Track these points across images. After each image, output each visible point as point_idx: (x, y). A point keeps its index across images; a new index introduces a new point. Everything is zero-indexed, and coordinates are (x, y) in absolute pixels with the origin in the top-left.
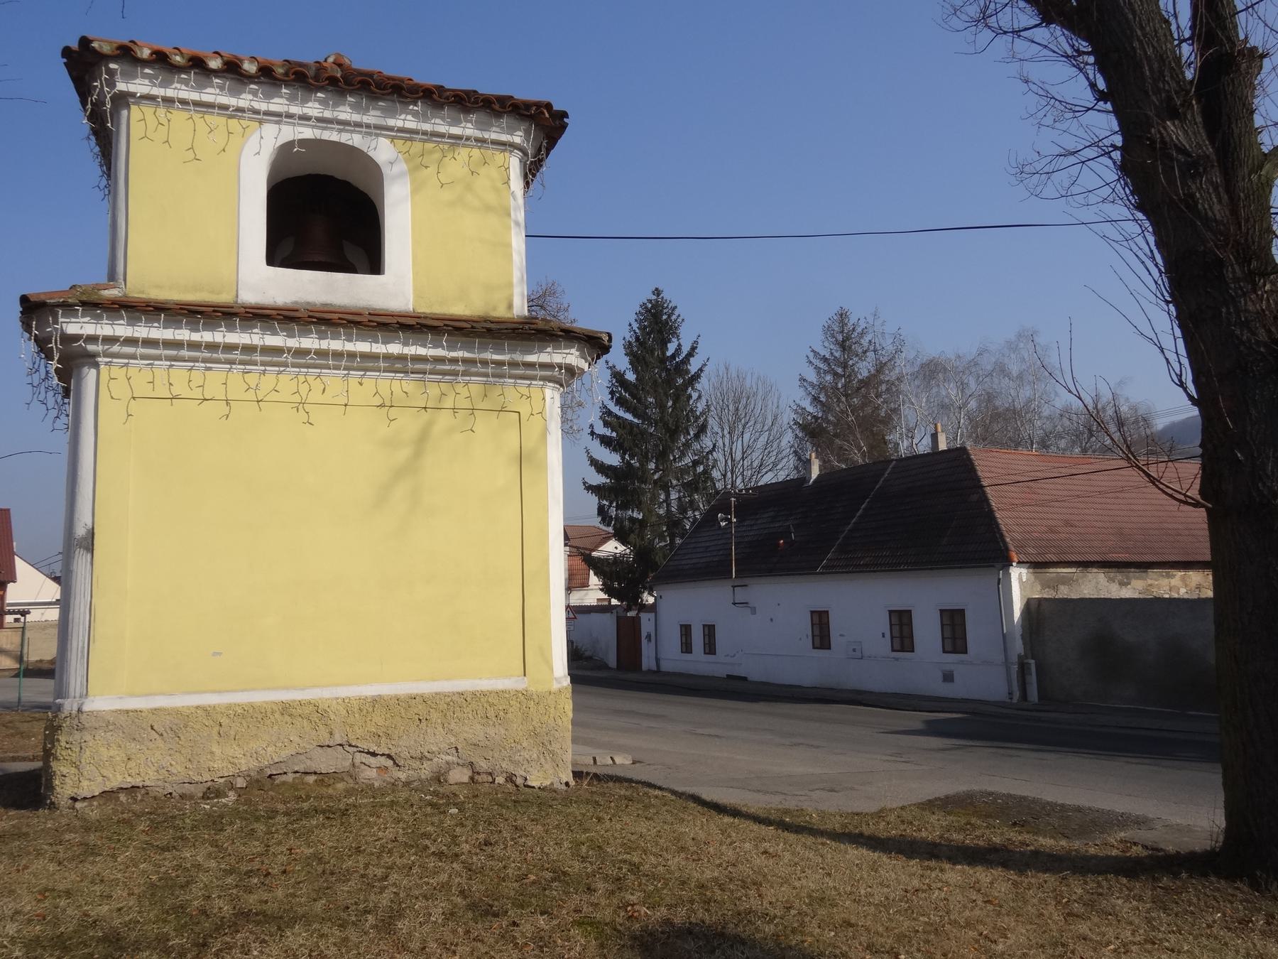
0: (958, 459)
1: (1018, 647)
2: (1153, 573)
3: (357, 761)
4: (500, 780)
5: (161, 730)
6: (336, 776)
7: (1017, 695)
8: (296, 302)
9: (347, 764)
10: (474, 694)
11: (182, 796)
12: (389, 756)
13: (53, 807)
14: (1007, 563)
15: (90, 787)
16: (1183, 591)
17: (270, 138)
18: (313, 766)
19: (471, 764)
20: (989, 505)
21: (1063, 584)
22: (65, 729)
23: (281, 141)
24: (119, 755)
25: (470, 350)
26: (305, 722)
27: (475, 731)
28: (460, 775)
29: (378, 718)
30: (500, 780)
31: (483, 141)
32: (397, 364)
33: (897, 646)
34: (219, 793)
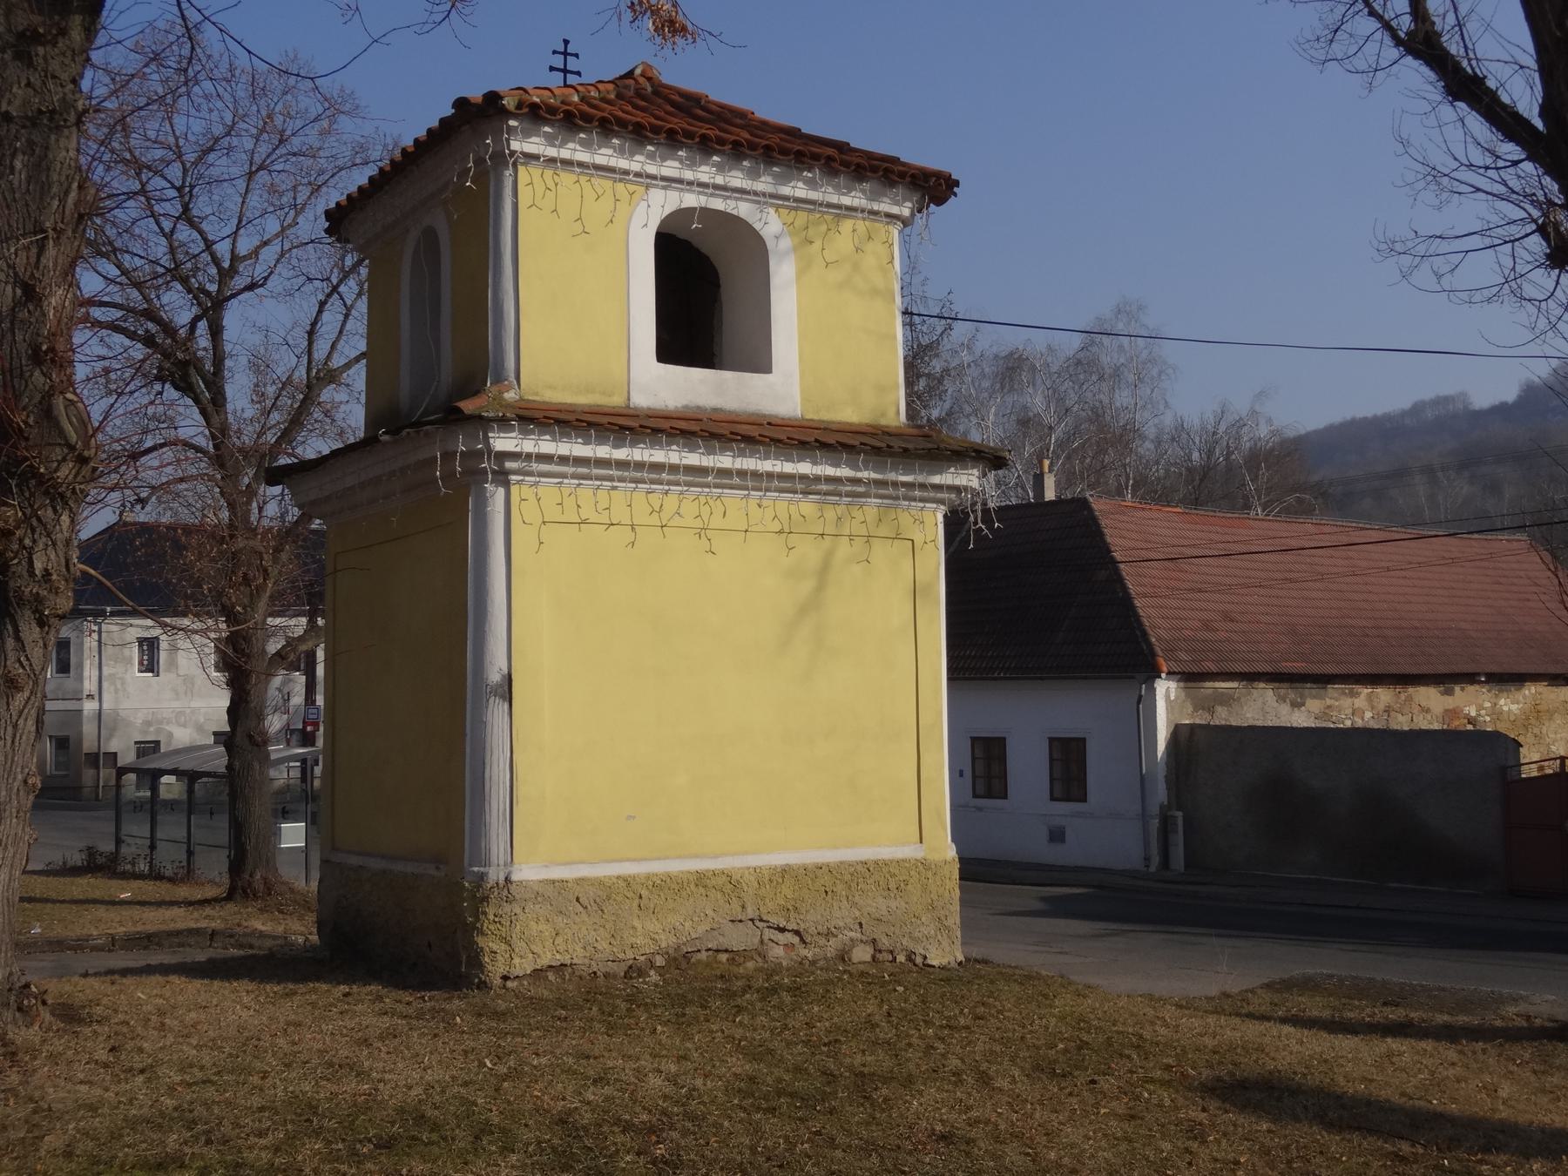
0: (1075, 519)
1: (1160, 793)
2: (1333, 690)
3: (766, 938)
4: (901, 958)
5: (586, 903)
6: (745, 954)
7: (1156, 860)
8: (686, 407)
9: (756, 940)
10: (876, 863)
11: (606, 975)
12: (797, 933)
13: (483, 986)
14: (1155, 673)
15: (523, 966)
16: (1368, 715)
17: (658, 206)
18: (725, 942)
19: (874, 941)
20: (1125, 589)
21: (1221, 704)
22: (493, 901)
23: (667, 211)
24: (547, 930)
25: (855, 468)
26: (719, 895)
27: (877, 904)
28: (862, 954)
29: (787, 890)
30: (901, 958)
31: (872, 212)
32: (807, 486)
33: (981, 789)
34: (641, 973)
